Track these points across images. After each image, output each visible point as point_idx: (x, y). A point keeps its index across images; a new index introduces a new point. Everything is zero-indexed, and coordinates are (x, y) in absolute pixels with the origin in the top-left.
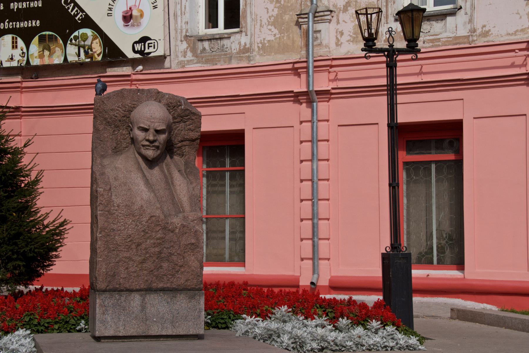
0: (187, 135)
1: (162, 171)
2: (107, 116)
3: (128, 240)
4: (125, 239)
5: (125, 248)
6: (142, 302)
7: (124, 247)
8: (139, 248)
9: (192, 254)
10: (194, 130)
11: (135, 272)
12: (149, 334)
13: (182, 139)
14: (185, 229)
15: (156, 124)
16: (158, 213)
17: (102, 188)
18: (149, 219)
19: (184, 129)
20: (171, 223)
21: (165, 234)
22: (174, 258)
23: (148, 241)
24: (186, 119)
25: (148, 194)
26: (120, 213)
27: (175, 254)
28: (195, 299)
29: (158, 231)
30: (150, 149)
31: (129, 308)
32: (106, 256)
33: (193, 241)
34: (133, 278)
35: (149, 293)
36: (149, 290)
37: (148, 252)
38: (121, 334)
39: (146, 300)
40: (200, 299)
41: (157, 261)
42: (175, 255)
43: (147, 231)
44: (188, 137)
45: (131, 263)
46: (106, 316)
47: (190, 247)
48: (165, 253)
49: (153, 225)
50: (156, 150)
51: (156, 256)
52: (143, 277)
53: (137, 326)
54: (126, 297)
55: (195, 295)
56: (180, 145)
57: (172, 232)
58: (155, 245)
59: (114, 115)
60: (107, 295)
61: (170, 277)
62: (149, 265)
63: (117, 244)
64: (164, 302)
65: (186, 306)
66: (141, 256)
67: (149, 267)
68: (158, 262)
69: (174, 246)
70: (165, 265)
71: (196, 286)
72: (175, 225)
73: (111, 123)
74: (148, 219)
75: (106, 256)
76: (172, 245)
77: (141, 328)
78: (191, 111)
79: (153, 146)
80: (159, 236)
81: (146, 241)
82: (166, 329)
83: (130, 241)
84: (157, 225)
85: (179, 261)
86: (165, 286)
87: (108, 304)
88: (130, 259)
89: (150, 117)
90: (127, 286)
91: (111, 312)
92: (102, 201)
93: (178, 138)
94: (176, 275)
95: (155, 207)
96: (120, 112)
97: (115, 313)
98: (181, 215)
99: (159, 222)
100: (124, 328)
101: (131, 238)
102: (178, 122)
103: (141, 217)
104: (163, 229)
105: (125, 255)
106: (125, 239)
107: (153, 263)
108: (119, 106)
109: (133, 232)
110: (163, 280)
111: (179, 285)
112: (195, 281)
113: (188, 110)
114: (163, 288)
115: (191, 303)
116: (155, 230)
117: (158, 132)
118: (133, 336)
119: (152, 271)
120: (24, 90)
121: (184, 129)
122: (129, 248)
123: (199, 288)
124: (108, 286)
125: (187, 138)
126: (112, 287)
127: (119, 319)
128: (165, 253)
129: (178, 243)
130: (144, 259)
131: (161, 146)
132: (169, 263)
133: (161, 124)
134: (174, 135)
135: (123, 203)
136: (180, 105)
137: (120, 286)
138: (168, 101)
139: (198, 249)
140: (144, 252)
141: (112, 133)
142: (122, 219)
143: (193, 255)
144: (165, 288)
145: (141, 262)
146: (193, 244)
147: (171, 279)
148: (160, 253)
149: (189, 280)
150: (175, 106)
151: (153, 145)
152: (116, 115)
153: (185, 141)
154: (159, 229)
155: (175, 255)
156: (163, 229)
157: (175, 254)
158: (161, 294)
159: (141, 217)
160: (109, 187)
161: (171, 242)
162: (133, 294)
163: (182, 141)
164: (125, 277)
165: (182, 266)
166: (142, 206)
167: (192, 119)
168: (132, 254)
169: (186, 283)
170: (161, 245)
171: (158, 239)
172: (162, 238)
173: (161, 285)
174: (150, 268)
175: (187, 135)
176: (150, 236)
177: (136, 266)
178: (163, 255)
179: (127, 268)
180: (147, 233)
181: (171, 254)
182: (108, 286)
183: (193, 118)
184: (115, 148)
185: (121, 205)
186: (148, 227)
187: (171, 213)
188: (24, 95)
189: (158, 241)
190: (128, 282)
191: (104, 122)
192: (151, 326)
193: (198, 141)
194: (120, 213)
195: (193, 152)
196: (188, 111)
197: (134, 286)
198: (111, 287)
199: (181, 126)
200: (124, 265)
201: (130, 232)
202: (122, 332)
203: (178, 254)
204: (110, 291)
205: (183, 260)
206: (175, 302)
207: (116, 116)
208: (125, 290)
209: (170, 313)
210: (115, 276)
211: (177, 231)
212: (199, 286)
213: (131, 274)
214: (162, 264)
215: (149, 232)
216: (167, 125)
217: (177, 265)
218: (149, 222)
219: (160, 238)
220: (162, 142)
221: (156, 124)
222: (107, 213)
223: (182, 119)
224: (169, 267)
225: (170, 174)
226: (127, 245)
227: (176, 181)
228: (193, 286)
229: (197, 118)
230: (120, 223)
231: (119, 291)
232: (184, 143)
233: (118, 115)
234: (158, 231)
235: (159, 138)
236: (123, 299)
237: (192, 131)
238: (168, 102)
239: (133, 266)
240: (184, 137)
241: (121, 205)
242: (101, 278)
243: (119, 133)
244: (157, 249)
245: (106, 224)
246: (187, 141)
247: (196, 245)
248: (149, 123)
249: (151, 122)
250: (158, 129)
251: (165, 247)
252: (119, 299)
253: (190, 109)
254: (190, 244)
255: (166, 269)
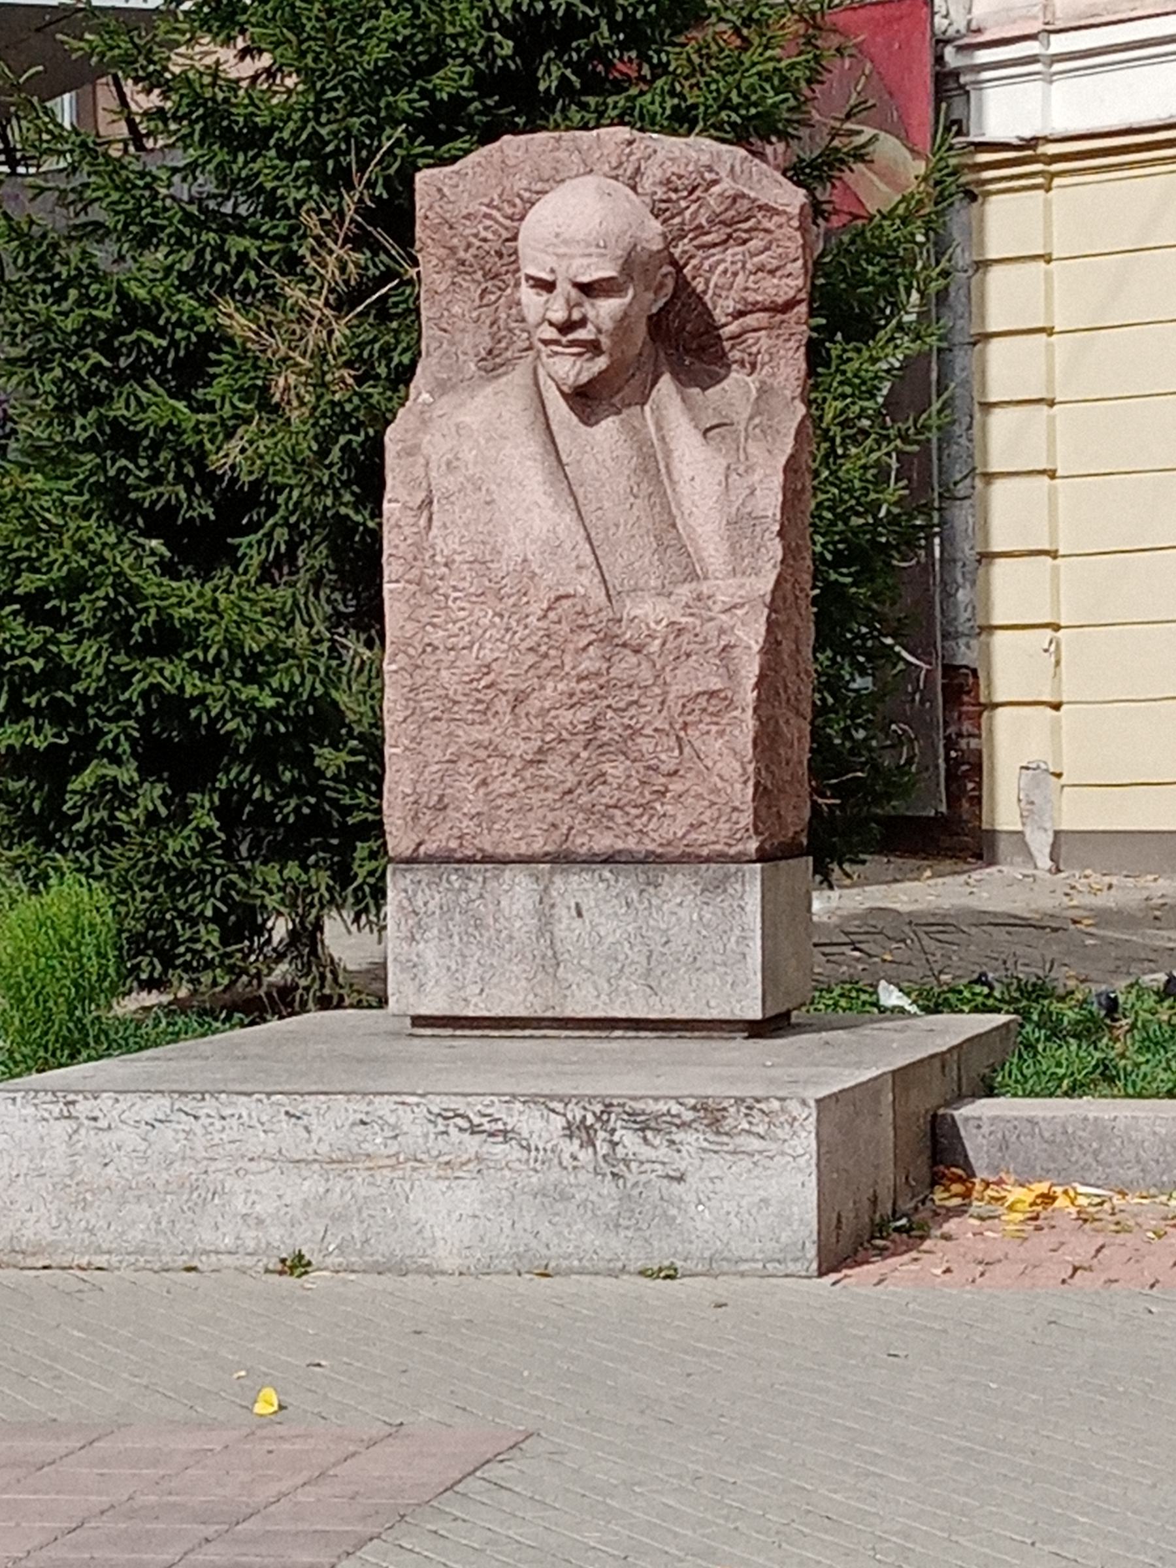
0: (755, 291)
1: (634, 433)
2: (455, 241)
3: (483, 683)
4: (472, 681)
5: (471, 711)
6: (541, 902)
7: (469, 707)
8: (521, 710)
9: (714, 728)
10: (778, 268)
11: (512, 795)
12: (568, 1013)
13: (739, 307)
14: (685, 638)
15: (577, 262)
16: (586, 583)
17: (397, 501)
18: (550, 608)
19: (743, 267)
20: (632, 621)
21: (609, 660)
22: (645, 744)
23: (550, 685)
24: (746, 231)
25: (553, 516)
26: (455, 589)
27: (648, 731)
28: (725, 891)
29: (585, 649)
30: (563, 354)
31: (496, 920)
32: (413, 740)
33: (715, 683)
34: (506, 816)
35: (563, 871)
36: (563, 859)
37: (550, 724)
38: (470, 1013)
39: (554, 894)
40: (744, 892)
41: (584, 755)
42: (647, 736)
43: (544, 648)
44: (760, 298)
45: (494, 761)
46: (422, 945)
47: (705, 704)
48: (611, 729)
49: (565, 627)
50: (587, 356)
51: (580, 737)
52: (540, 812)
53: (524, 983)
54: (484, 882)
55: (727, 876)
56: (734, 328)
57: (637, 652)
58: (575, 699)
59: (476, 236)
60: (422, 873)
61: (634, 812)
62: (555, 768)
63: (447, 696)
64: (615, 901)
65: (695, 917)
66: (529, 739)
67: (561, 778)
68: (589, 759)
69: (643, 701)
70: (616, 770)
71: (730, 845)
72: (647, 625)
73: (471, 266)
74: (545, 606)
75: (413, 740)
76: (635, 698)
77: (539, 991)
78: (754, 200)
79: (572, 343)
80: (586, 666)
81: (543, 687)
82: (624, 999)
83: (487, 687)
84: (581, 627)
85: (663, 757)
86: (620, 845)
87: (426, 904)
88: (492, 748)
89: (555, 241)
90: (487, 843)
91: (435, 931)
92: (396, 547)
93: (726, 303)
94: (658, 806)
95: (573, 565)
96: (497, 222)
97: (451, 937)
98: (685, 592)
99: (587, 616)
100: (482, 990)
101: (492, 676)
102: (715, 245)
103: (525, 599)
104: (602, 640)
105: (475, 736)
106: (472, 681)
107: (571, 762)
108: (492, 200)
109: (496, 655)
110: (611, 824)
111: (669, 843)
112: (724, 827)
113: (744, 196)
114: (610, 852)
115: (711, 909)
116: (571, 646)
117: (588, 289)
118: (511, 1020)
119: (570, 792)
120: (1057, 67)
121: (743, 267)
122: (486, 711)
123: (740, 853)
124: (420, 844)
125: (757, 302)
126: (435, 846)
127: (463, 956)
128: (611, 729)
129: (657, 690)
130: (540, 751)
131: (605, 341)
132: (628, 763)
133: (594, 259)
134: (710, 292)
135: (463, 552)
136: (715, 182)
137: (461, 845)
138: (664, 171)
139: (735, 713)
140: (537, 724)
141: (477, 303)
142: (463, 609)
143: (721, 733)
144: (620, 852)
145: (531, 762)
146: (712, 694)
147: (637, 821)
148: (594, 725)
149: (704, 823)
150: (694, 189)
151: (571, 337)
152: (483, 234)
153: (751, 312)
154: (586, 642)
155: (647, 736)
156: (602, 640)
157: (648, 731)
158: (607, 874)
159: (525, 599)
160: (421, 495)
161: (630, 686)
162: (508, 872)
163: (741, 314)
164: (478, 814)
165: (676, 772)
166: (525, 560)
167: (767, 231)
168: (499, 731)
169: (693, 836)
170: (596, 697)
171: (580, 679)
172: (598, 674)
173: (604, 842)
174: (562, 782)
175: (755, 291)
176: (556, 667)
177: (514, 776)
178: (605, 736)
179: (484, 783)
180: (546, 656)
181: (636, 732)
182: (420, 844)
183: (770, 225)
184: (490, 352)
185: (458, 558)
186: (548, 636)
187: (641, 583)
188: (1060, 87)
189: (584, 685)
190: (490, 830)
191: (451, 262)
192: (574, 987)
193: (803, 309)
194: (455, 589)
195: (791, 353)
196: (746, 201)
197: (510, 846)
198: (430, 847)
199: (729, 259)
200: (471, 770)
201: (487, 655)
202: (476, 1005)
203: (656, 730)
204: (430, 859)
205: (676, 753)
206: (655, 901)
207: (485, 240)
208: (479, 857)
209: (639, 939)
210: (445, 808)
211: (655, 646)
212: (740, 847)
213: (499, 802)
214: (606, 767)
215: (552, 652)
216: (620, 262)
217: (656, 769)
218: (552, 615)
219: (590, 673)
220: (608, 325)
221: (577, 262)
222: (413, 587)
223: (729, 230)
224: (629, 777)
225: (663, 439)
226: (479, 701)
227: (679, 466)
228: (718, 847)
229: (780, 226)
230: (455, 622)
231: (459, 861)
232: (750, 320)
233: (490, 236)
234: (585, 649)
235: (591, 314)
236: (474, 888)
237: (772, 272)
238: (668, 174)
239: (504, 774)
240: (745, 299)
241: (458, 558)
242: (398, 814)
243: (502, 300)
244: (585, 714)
245: (410, 627)
246: (760, 310)
247: (725, 698)
248: (551, 262)
249: (557, 255)
250: (585, 279)
251: (609, 707)
252: (460, 890)
253: (753, 194)
254: (704, 693)
255: (619, 787)
